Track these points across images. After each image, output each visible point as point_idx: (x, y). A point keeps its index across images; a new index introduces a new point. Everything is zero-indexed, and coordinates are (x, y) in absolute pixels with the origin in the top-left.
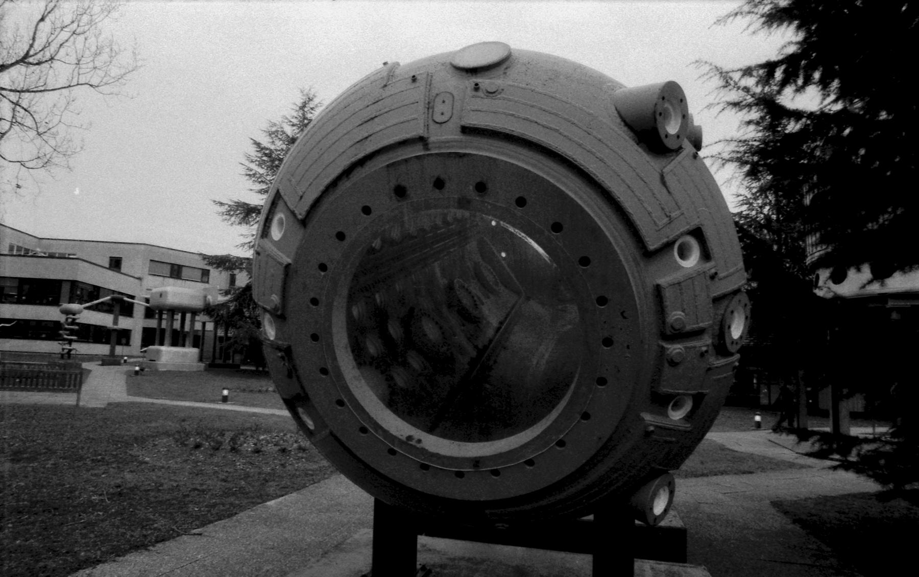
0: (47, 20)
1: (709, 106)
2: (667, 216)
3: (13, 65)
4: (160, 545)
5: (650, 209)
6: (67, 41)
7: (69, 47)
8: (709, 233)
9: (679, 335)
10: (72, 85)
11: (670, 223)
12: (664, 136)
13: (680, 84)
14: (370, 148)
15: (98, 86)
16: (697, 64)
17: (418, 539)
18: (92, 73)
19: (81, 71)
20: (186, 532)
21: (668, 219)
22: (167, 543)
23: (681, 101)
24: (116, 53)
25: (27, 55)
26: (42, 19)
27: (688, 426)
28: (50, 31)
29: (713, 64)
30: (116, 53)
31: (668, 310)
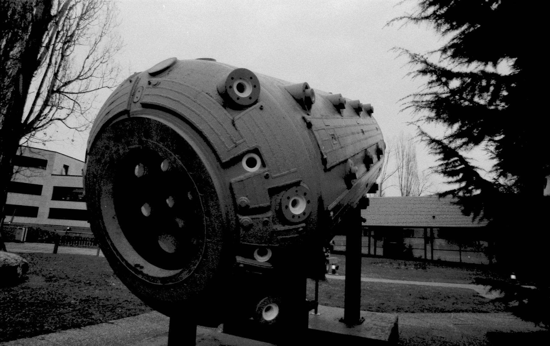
0: (90, 58)
1: (410, 74)
2: (234, 143)
3: (74, 80)
4: (88, 327)
5: (223, 140)
6: (98, 67)
7: (99, 69)
8: (262, 151)
9: (246, 210)
10: (100, 88)
11: (236, 147)
12: (236, 99)
13: (249, 69)
14: (110, 116)
15: (111, 88)
16: (394, 49)
17: (197, 330)
18: (109, 81)
19: (104, 81)
20: (106, 322)
21: (234, 145)
22: (93, 326)
23: (251, 78)
24: (121, 70)
25: (79, 77)
26: (88, 58)
27: (269, 265)
28: (91, 63)
29: (404, 49)
30: (121, 70)
31: (237, 196)
